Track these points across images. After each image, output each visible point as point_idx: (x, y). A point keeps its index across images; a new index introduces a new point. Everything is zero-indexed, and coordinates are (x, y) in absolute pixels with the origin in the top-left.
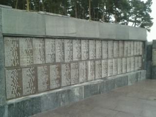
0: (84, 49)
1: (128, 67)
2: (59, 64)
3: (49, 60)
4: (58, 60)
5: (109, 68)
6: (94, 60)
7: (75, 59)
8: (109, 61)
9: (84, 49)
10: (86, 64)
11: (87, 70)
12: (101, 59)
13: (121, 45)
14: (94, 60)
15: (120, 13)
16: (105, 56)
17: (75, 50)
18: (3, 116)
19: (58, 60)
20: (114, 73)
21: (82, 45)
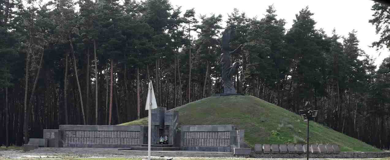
0: (213, 135)
1: (220, 144)
2: (194, 139)
3: (192, 138)
4: (194, 138)
5: (210, 143)
6: (204, 139)
7: (196, 138)
8: (210, 140)
9: (213, 135)
10: (202, 140)
11: (202, 142)
12: (219, 139)
13: (216, 134)
14: (204, 139)
15: (387, 73)
16: (209, 138)
17: (198, 136)
18: (389, 153)
19: (194, 138)
20: (213, 145)
21: (126, 143)
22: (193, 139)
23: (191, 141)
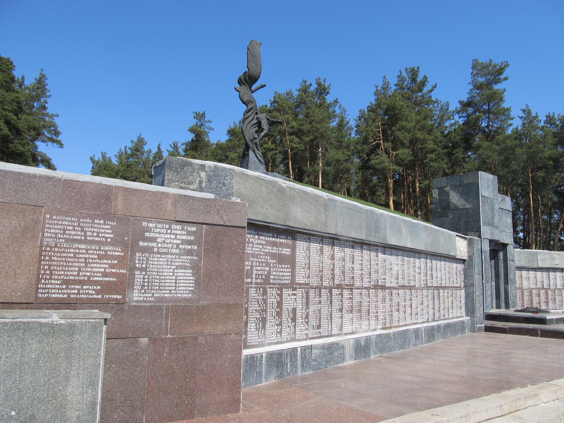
19: (545, 286)
22: (543, 288)
23: (539, 295)
